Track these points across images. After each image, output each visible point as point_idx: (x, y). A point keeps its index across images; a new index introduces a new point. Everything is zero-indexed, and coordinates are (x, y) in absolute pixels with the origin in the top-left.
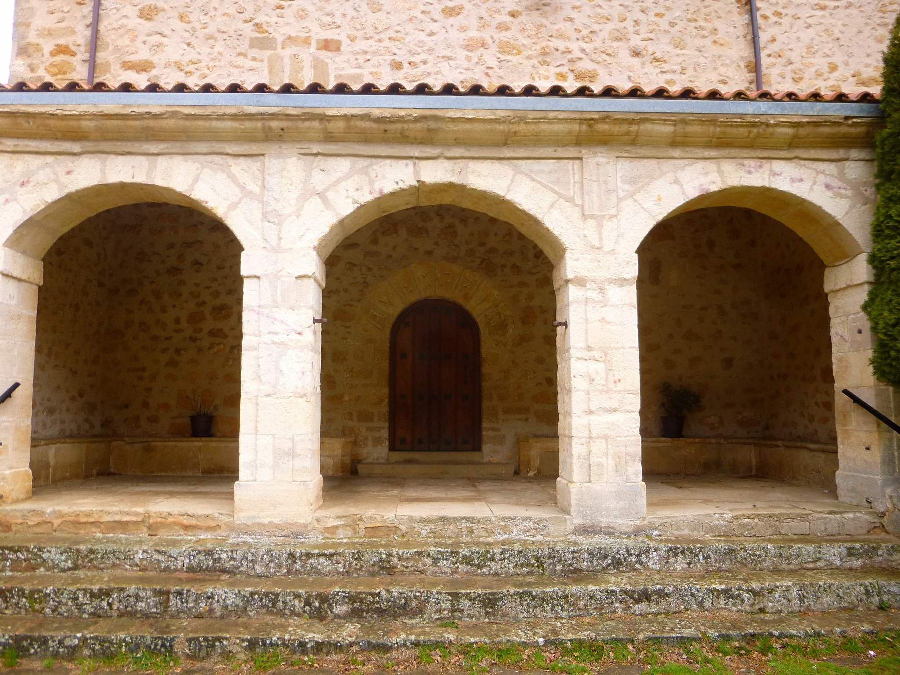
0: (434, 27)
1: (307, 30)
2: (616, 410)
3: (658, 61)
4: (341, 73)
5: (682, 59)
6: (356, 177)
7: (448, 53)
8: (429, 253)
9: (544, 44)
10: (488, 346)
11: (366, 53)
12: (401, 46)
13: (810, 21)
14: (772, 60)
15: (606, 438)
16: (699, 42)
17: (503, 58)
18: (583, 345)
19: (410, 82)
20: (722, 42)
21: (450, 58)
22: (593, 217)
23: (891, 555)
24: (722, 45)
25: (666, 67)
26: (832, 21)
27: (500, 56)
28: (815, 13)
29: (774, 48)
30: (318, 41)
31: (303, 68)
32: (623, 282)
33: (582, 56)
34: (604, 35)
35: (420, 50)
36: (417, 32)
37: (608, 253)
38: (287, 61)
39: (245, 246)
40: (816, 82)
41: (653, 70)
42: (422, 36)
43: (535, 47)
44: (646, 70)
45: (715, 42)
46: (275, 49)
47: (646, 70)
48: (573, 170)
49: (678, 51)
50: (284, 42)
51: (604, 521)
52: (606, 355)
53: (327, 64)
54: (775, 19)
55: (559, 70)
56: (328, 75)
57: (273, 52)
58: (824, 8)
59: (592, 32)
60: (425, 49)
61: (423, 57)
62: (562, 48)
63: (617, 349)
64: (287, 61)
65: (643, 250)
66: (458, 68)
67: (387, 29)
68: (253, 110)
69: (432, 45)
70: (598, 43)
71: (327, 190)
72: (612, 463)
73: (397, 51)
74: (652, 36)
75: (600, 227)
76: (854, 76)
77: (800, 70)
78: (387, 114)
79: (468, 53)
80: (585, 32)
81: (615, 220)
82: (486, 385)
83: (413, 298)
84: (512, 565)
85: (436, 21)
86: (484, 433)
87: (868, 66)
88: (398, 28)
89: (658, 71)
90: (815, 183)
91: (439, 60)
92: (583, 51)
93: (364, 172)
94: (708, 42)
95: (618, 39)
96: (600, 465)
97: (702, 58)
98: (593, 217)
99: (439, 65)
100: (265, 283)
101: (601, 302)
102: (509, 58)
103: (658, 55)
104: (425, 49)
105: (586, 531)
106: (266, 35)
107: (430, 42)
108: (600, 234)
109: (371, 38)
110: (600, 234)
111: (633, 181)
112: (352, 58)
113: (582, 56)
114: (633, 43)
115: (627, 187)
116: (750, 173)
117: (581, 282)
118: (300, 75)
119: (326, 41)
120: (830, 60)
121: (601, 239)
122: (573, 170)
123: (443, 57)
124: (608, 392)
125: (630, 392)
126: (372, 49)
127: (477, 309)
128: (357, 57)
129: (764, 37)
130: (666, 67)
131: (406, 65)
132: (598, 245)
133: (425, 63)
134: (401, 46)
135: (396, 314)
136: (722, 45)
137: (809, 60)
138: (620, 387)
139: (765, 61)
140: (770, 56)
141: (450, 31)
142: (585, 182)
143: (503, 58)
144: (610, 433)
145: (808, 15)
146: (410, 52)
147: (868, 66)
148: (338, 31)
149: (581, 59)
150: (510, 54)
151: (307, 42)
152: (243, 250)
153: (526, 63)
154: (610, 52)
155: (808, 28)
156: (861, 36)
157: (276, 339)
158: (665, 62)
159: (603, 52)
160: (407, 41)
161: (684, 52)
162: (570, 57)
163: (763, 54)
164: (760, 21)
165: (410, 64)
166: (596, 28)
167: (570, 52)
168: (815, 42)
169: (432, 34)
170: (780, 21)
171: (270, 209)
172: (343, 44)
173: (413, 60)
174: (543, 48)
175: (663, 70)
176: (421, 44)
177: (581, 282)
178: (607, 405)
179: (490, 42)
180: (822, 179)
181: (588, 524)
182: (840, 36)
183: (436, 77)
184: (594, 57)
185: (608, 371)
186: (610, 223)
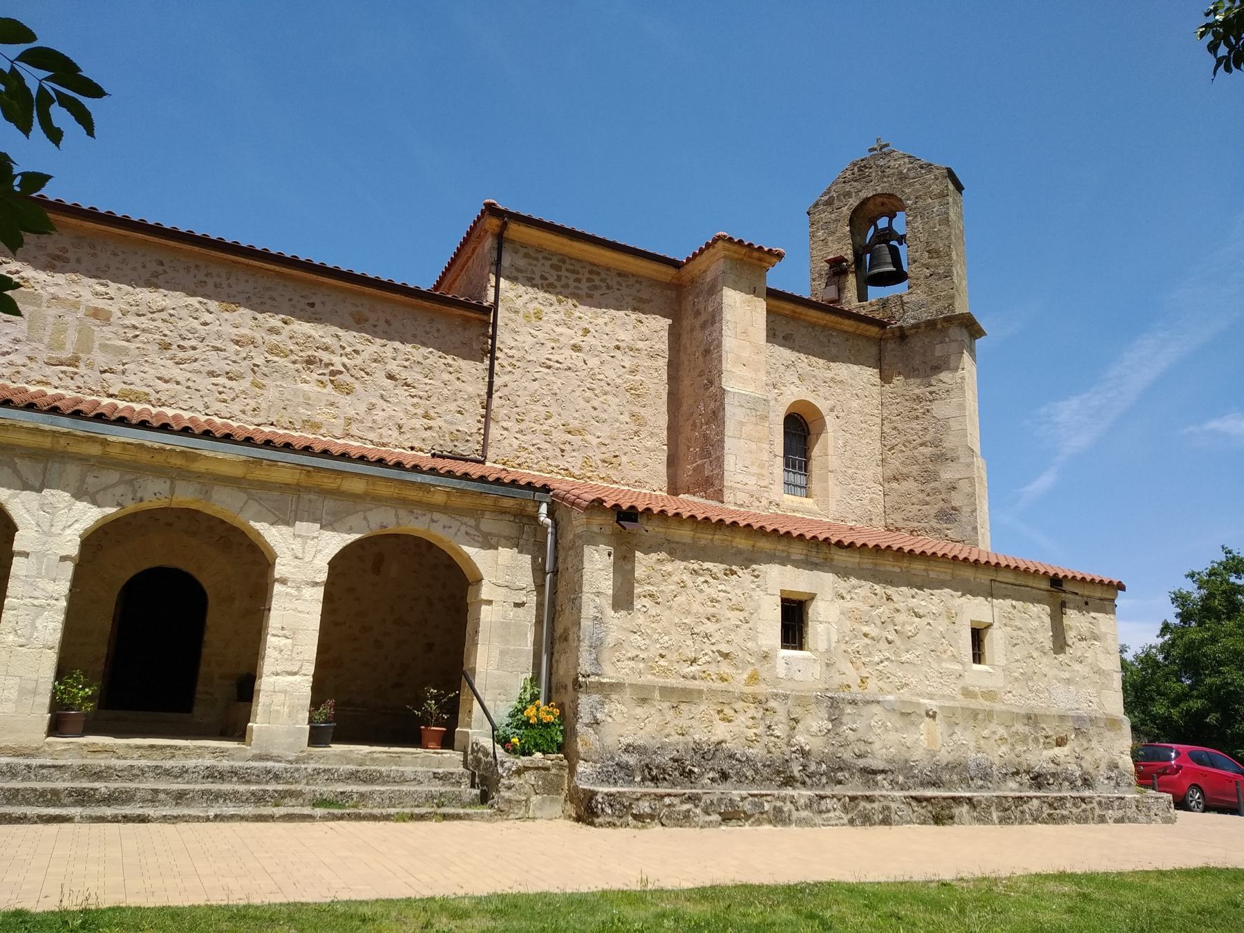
0: (207, 317)
1: (77, 295)
2: (295, 674)
3: (408, 386)
4: (107, 342)
5: (429, 387)
6: (122, 486)
7: (218, 344)
8: (170, 525)
9: (310, 353)
10: (214, 616)
11: (135, 327)
12: (172, 328)
13: (537, 375)
14: (503, 402)
15: (285, 692)
16: (446, 376)
17: (270, 357)
18: (279, 626)
19: (177, 363)
20: (464, 379)
21: (217, 349)
22: (299, 536)
23: (461, 779)
24: (463, 382)
25: (414, 392)
26: (553, 378)
27: (267, 355)
28: (541, 369)
29: (505, 391)
30: (87, 307)
31: (67, 329)
32: (316, 584)
33: (343, 369)
34: (365, 355)
35: (190, 336)
36: (191, 319)
37: (307, 563)
38: (51, 320)
39: (19, 526)
40: (533, 425)
41: (403, 392)
42: (196, 324)
43: (301, 354)
44: (396, 392)
45: (458, 379)
46: (39, 306)
47: (396, 392)
48: (292, 501)
49: (427, 380)
50: (48, 301)
51: (275, 752)
52: (294, 633)
53: (94, 331)
54: (510, 369)
55: (320, 378)
56: (93, 341)
57: (35, 308)
58: (549, 367)
59: (354, 351)
60: (196, 335)
61: (193, 343)
62: (326, 360)
63: (302, 630)
64: (51, 320)
65: (333, 564)
66: (226, 359)
67: (162, 310)
68: (47, 427)
69: (203, 334)
70: (358, 360)
71: (97, 492)
72: (286, 710)
73: (167, 332)
74: (406, 364)
75: (305, 544)
76: (564, 425)
77: (523, 413)
78: (156, 445)
79: (237, 347)
80: (348, 350)
81: (316, 540)
82: (205, 651)
83: (146, 566)
84: (201, 776)
85: (211, 313)
86: (197, 696)
87: (575, 418)
88: (172, 312)
89: (407, 394)
90: (459, 530)
91: (207, 348)
92: (344, 366)
93: (130, 483)
94: (452, 378)
95: (375, 361)
96: (278, 711)
97: (446, 390)
98: (299, 536)
99: (207, 353)
100: (32, 558)
101: (296, 596)
102: (276, 359)
103: (409, 381)
104: (196, 335)
105: (260, 758)
106: (32, 290)
107: (202, 330)
108: (304, 548)
109: (144, 315)
110: (304, 548)
111: (334, 514)
112: (121, 331)
113: (343, 369)
114: (389, 367)
115: (329, 518)
116: (417, 518)
117: (283, 581)
118: (62, 337)
119: (96, 309)
120: (547, 410)
121: (304, 552)
122: (292, 501)
123: (213, 347)
124: (291, 660)
125: (308, 661)
126: (143, 326)
127: (207, 580)
128: (126, 330)
129: (498, 381)
130: (414, 392)
131: (174, 347)
132: (300, 556)
133: (194, 348)
134: (172, 328)
135: (127, 578)
136: (463, 382)
137: (531, 406)
138: (301, 657)
139: (496, 401)
140: (501, 398)
141: (223, 324)
142: (299, 512)
143: (270, 357)
144: (289, 689)
145: (536, 370)
146: (180, 336)
147: (575, 418)
148: (110, 302)
149: (341, 373)
150: (277, 355)
151: (75, 306)
152: (17, 530)
153: (291, 365)
154: (368, 370)
155: (534, 380)
156: (574, 394)
157: (36, 602)
158: (414, 387)
159: (362, 370)
160: (179, 324)
161: (431, 381)
162: (331, 368)
163: (495, 396)
164: (497, 368)
165: (179, 346)
166: (360, 347)
167: (332, 365)
168: (538, 393)
169: (205, 324)
170: (514, 371)
171: (46, 502)
172: (114, 315)
173: (182, 343)
174: (309, 356)
175: (412, 394)
176: (193, 331)
177: (283, 581)
178: (289, 669)
179: (260, 341)
180: (464, 528)
181: (264, 753)
182: (558, 391)
183: (202, 363)
184: (353, 372)
185: (294, 645)
186: (312, 542)
